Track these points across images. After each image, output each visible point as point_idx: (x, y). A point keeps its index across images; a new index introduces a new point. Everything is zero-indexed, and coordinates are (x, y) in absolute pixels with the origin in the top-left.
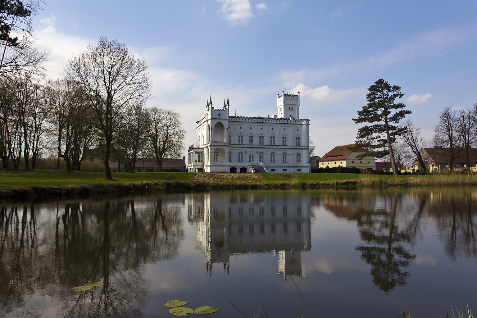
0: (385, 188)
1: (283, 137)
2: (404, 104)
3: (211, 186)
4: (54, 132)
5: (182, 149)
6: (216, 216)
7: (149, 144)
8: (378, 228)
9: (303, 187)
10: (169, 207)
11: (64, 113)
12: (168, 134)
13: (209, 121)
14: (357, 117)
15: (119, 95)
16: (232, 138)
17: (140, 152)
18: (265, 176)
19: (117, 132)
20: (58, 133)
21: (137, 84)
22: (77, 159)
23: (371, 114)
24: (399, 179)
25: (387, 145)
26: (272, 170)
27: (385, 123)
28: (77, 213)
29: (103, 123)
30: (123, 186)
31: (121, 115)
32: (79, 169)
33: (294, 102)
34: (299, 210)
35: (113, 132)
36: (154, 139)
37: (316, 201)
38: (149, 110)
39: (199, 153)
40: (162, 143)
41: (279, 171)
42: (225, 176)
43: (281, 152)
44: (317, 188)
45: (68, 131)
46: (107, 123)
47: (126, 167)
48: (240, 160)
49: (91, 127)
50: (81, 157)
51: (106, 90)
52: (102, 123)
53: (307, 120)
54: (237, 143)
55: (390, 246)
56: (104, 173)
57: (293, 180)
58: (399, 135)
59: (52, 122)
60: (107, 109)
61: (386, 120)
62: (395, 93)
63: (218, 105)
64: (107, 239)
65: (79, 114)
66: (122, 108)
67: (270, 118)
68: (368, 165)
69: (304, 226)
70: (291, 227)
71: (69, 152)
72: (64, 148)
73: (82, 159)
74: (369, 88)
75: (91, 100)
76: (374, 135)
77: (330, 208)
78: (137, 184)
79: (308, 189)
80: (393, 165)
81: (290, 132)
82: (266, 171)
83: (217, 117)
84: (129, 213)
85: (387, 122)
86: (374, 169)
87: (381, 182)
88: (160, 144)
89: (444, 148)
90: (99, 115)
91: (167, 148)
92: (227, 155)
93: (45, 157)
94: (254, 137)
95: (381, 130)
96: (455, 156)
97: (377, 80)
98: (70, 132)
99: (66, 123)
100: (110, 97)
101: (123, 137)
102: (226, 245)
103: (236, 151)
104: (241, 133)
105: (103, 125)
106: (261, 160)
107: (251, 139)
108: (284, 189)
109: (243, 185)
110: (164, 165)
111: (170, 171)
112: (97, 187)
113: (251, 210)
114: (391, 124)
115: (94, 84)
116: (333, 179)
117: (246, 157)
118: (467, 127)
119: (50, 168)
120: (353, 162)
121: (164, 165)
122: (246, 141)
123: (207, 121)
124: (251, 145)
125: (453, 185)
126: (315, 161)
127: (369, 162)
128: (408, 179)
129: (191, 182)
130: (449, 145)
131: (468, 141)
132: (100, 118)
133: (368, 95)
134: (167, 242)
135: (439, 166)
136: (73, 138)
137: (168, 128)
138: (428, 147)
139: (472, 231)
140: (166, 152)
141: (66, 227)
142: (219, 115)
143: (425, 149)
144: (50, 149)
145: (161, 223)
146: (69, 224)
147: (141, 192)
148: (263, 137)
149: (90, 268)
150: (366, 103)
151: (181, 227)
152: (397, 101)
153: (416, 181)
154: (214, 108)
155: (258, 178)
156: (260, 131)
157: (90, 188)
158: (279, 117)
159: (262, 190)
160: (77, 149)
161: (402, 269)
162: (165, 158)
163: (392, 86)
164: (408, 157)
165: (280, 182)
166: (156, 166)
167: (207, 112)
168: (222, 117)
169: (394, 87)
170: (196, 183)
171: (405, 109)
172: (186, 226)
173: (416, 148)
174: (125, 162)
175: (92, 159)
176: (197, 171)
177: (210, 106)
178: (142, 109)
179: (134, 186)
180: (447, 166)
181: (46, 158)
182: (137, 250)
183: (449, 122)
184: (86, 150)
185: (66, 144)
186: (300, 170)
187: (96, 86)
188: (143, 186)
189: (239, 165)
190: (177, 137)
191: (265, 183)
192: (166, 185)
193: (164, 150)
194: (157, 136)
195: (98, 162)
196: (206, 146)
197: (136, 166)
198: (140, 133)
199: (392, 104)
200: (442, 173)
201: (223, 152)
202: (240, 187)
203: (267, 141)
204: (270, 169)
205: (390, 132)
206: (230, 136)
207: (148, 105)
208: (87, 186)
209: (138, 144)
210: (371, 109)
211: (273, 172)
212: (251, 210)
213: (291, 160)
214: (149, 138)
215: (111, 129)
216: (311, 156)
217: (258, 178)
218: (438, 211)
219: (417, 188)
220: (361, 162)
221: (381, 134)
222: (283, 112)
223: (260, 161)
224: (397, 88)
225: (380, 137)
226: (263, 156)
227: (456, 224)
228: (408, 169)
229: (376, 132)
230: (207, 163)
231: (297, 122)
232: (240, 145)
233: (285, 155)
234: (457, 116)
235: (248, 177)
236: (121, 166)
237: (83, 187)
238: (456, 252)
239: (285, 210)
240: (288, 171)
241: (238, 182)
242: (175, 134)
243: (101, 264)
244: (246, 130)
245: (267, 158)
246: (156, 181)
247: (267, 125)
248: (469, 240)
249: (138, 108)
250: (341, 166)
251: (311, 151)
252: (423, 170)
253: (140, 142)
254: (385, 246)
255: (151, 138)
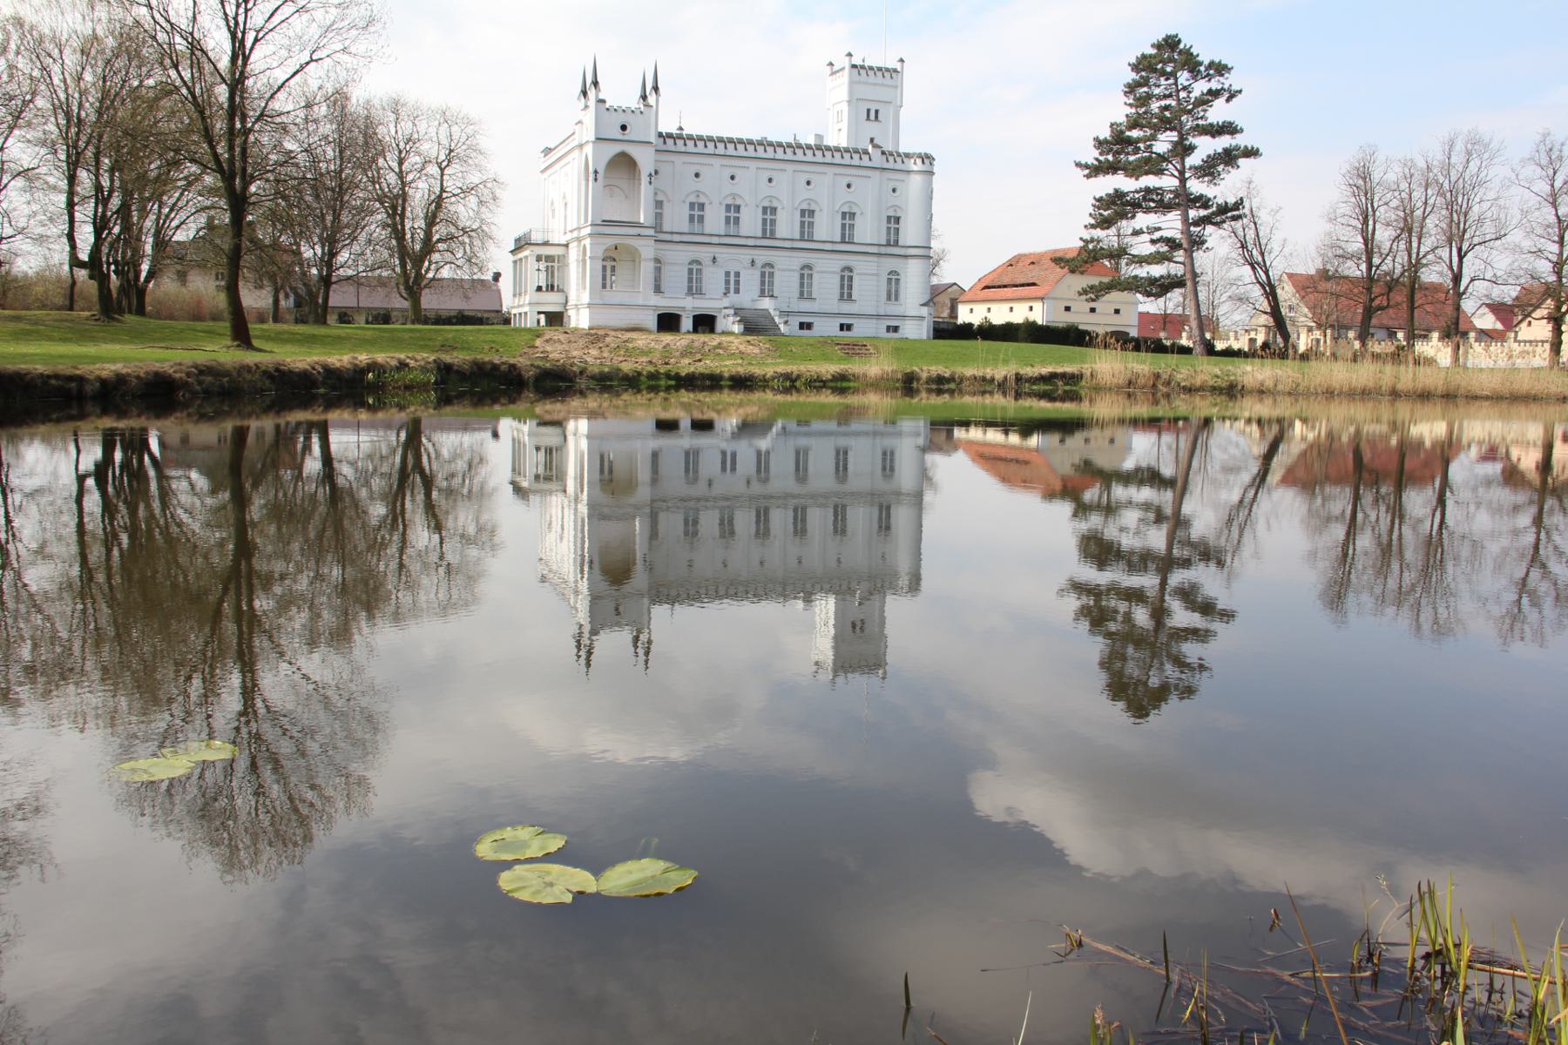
0: (1167, 396)
1: (844, 214)
2: (1239, 123)
3: (593, 377)
4: (52, 180)
5: (490, 244)
6: (609, 478)
7: (375, 225)
8: (1132, 528)
9: (909, 385)
10: (448, 443)
11: (83, 114)
12: (443, 190)
13: (589, 149)
14: (1091, 155)
15: (272, 48)
16: (667, 211)
17: (343, 257)
18: (781, 346)
19: (267, 180)
20: (64, 184)
21: (333, 11)
22: (131, 275)
23: (1136, 151)
24: (1210, 368)
25: (1180, 255)
26: (802, 326)
27: (1176, 182)
28: (141, 461)
29: (220, 150)
30: (291, 372)
31: (278, 120)
32: (141, 311)
33: (882, 94)
34: (888, 463)
35: (253, 179)
36: (394, 208)
37: (943, 430)
38: (376, 102)
39: (549, 258)
40: (421, 223)
41: (826, 328)
42: (641, 341)
43: (835, 264)
44: (951, 392)
45: (97, 175)
46: (231, 148)
47: (298, 304)
48: (694, 289)
49: (176, 164)
50: (145, 267)
51: (225, 29)
52: (213, 148)
53: (927, 158)
54: (685, 227)
55: (1163, 583)
56: (225, 326)
57: (873, 360)
58: (1216, 224)
59: (43, 143)
60: (232, 98)
61: (1182, 172)
62: (1214, 85)
63: (621, 92)
64: (245, 549)
65: (133, 115)
66: (281, 95)
67: (799, 146)
68: (1116, 319)
69: (901, 516)
70: (860, 518)
71: (105, 250)
72: (86, 236)
73: (151, 274)
74: (1133, 61)
75: (176, 66)
76: (1142, 220)
77: (989, 459)
78: (338, 365)
79: (924, 394)
80: (1194, 324)
81: (868, 196)
82: (782, 327)
83: (618, 134)
84: (313, 465)
85: (1183, 181)
86: (1134, 333)
87: (1157, 376)
88: (415, 223)
89: (1346, 278)
90: (204, 119)
91: (439, 241)
92: (647, 269)
93: (25, 268)
94: (707, 207)
95: (1164, 207)
96: (1376, 303)
97: (1161, 37)
98: (106, 183)
99: (91, 148)
100: (240, 53)
101: (285, 198)
102: (640, 579)
103: (678, 258)
104: (698, 193)
105: (216, 156)
106: (766, 290)
107: (732, 214)
108: (842, 391)
109: (703, 377)
110: (429, 301)
111: (448, 321)
112: (201, 372)
113: (729, 462)
114: (1196, 186)
115: (182, 7)
116: (1006, 362)
117: (713, 279)
118: (1418, 213)
119: (44, 307)
120: (1068, 309)
121: (429, 301)
122: (714, 221)
123: (581, 146)
124: (731, 239)
125: (1364, 394)
126: (945, 299)
127: (1117, 311)
128: (1239, 372)
129: (521, 361)
130: (1364, 267)
131: (1418, 260)
132: (206, 129)
133: (1128, 85)
134: (441, 558)
135: (1329, 332)
136: (115, 202)
137: (442, 170)
138: (1300, 270)
139: (1400, 535)
140: (436, 257)
141: (108, 508)
142: (624, 128)
143: (1290, 276)
144: (41, 239)
145: (420, 497)
146: (118, 494)
147: (353, 390)
148: (774, 210)
149: (196, 640)
150: (1119, 110)
151: (485, 517)
152: (1217, 113)
153: (1260, 377)
154: (603, 101)
155: (756, 351)
156: (765, 190)
157: (178, 375)
158: (830, 141)
159: (769, 396)
160: (131, 236)
161: (1191, 650)
162: (430, 275)
163: (1206, 62)
164: (1240, 299)
165: (828, 369)
166: (400, 303)
167: (581, 115)
168: (629, 135)
169: (1211, 65)
170: (540, 363)
171: (1240, 141)
172: (506, 511)
173: (1266, 273)
174: (294, 290)
175: (182, 277)
176: (543, 322)
177: (592, 93)
178: (354, 101)
179: (330, 372)
180: (1351, 334)
181: (30, 272)
182: (343, 589)
183: (1368, 193)
184: (161, 243)
185: (94, 223)
186: (896, 329)
187: (190, 14)
188: (360, 372)
189: (688, 307)
190: (472, 201)
191: (781, 369)
192: (439, 368)
193: (428, 247)
194: (404, 196)
195: (205, 287)
196: (575, 234)
197: (331, 303)
198: (342, 189)
199: (1200, 122)
200: (1334, 356)
201: (634, 257)
202: (690, 382)
203: (787, 226)
204: (795, 321)
205: (1193, 213)
206: (659, 204)
207: (370, 89)
208: (167, 368)
209: (337, 226)
210: (1135, 134)
211: (805, 332)
212: (729, 462)
213: (868, 292)
214: (377, 205)
215: (244, 170)
216: (935, 281)
217: (756, 351)
218: (1309, 476)
219: (1261, 400)
220: (1093, 310)
221: (1163, 218)
222: (844, 125)
223: (762, 294)
224: (1220, 69)
225: (1159, 229)
226: (771, 275)
227: (1360, 516)
228: (1236, 339)
229: (1148, 210)
230: (578, 297)
231: (892, 162)
232: (696, 235)
233: (847, 274)
234: (1391, 177)
235: (720, 346)
236: (283, 303)
237: (157, 374)
238: (1351, 598)
239: (841, 460)
240: (815, 328)
241: (685, 366)
242: (466, 191)
243: (229, 627)
244: (715, 184)
245: (787, 283)
246: (402, 356)
247: (790, 167)
248: (1389, 565)
249: (338, 99)
250: (1031, 319)
251: (936, 265)
252: (1278, 345)
253: (345, 218)
254: (1147, 581)
255: (382, 203)
